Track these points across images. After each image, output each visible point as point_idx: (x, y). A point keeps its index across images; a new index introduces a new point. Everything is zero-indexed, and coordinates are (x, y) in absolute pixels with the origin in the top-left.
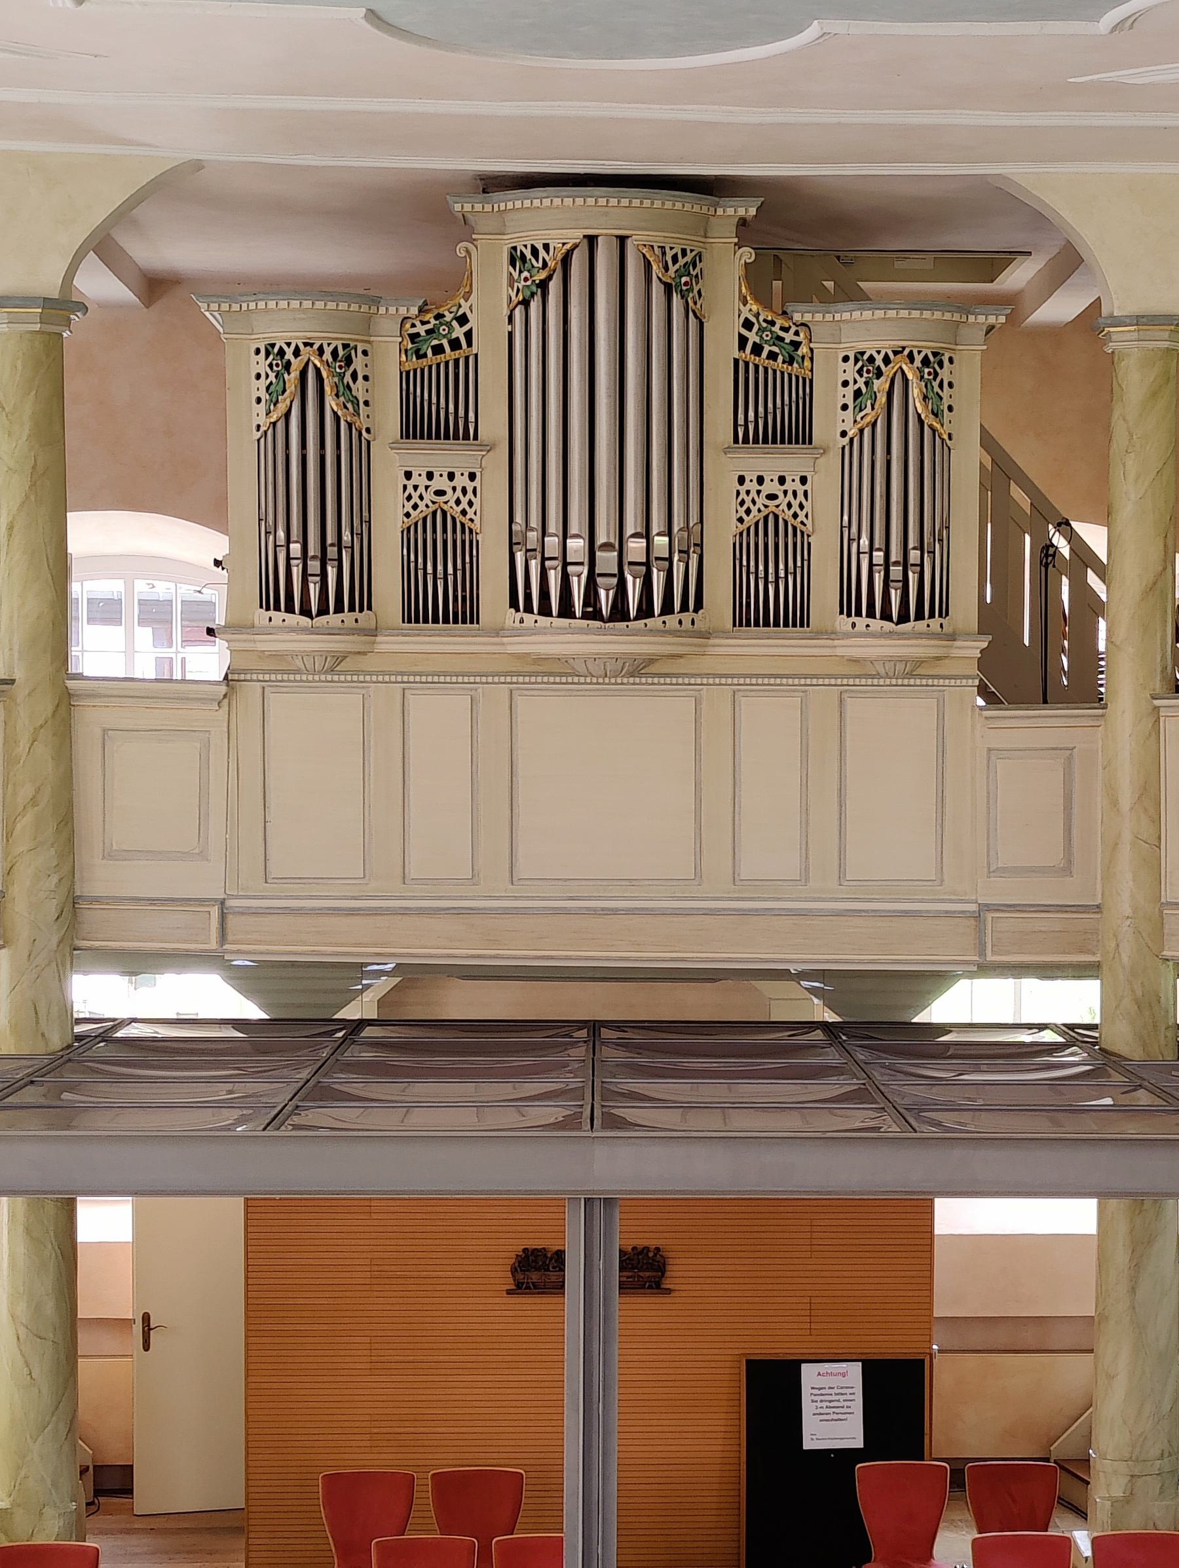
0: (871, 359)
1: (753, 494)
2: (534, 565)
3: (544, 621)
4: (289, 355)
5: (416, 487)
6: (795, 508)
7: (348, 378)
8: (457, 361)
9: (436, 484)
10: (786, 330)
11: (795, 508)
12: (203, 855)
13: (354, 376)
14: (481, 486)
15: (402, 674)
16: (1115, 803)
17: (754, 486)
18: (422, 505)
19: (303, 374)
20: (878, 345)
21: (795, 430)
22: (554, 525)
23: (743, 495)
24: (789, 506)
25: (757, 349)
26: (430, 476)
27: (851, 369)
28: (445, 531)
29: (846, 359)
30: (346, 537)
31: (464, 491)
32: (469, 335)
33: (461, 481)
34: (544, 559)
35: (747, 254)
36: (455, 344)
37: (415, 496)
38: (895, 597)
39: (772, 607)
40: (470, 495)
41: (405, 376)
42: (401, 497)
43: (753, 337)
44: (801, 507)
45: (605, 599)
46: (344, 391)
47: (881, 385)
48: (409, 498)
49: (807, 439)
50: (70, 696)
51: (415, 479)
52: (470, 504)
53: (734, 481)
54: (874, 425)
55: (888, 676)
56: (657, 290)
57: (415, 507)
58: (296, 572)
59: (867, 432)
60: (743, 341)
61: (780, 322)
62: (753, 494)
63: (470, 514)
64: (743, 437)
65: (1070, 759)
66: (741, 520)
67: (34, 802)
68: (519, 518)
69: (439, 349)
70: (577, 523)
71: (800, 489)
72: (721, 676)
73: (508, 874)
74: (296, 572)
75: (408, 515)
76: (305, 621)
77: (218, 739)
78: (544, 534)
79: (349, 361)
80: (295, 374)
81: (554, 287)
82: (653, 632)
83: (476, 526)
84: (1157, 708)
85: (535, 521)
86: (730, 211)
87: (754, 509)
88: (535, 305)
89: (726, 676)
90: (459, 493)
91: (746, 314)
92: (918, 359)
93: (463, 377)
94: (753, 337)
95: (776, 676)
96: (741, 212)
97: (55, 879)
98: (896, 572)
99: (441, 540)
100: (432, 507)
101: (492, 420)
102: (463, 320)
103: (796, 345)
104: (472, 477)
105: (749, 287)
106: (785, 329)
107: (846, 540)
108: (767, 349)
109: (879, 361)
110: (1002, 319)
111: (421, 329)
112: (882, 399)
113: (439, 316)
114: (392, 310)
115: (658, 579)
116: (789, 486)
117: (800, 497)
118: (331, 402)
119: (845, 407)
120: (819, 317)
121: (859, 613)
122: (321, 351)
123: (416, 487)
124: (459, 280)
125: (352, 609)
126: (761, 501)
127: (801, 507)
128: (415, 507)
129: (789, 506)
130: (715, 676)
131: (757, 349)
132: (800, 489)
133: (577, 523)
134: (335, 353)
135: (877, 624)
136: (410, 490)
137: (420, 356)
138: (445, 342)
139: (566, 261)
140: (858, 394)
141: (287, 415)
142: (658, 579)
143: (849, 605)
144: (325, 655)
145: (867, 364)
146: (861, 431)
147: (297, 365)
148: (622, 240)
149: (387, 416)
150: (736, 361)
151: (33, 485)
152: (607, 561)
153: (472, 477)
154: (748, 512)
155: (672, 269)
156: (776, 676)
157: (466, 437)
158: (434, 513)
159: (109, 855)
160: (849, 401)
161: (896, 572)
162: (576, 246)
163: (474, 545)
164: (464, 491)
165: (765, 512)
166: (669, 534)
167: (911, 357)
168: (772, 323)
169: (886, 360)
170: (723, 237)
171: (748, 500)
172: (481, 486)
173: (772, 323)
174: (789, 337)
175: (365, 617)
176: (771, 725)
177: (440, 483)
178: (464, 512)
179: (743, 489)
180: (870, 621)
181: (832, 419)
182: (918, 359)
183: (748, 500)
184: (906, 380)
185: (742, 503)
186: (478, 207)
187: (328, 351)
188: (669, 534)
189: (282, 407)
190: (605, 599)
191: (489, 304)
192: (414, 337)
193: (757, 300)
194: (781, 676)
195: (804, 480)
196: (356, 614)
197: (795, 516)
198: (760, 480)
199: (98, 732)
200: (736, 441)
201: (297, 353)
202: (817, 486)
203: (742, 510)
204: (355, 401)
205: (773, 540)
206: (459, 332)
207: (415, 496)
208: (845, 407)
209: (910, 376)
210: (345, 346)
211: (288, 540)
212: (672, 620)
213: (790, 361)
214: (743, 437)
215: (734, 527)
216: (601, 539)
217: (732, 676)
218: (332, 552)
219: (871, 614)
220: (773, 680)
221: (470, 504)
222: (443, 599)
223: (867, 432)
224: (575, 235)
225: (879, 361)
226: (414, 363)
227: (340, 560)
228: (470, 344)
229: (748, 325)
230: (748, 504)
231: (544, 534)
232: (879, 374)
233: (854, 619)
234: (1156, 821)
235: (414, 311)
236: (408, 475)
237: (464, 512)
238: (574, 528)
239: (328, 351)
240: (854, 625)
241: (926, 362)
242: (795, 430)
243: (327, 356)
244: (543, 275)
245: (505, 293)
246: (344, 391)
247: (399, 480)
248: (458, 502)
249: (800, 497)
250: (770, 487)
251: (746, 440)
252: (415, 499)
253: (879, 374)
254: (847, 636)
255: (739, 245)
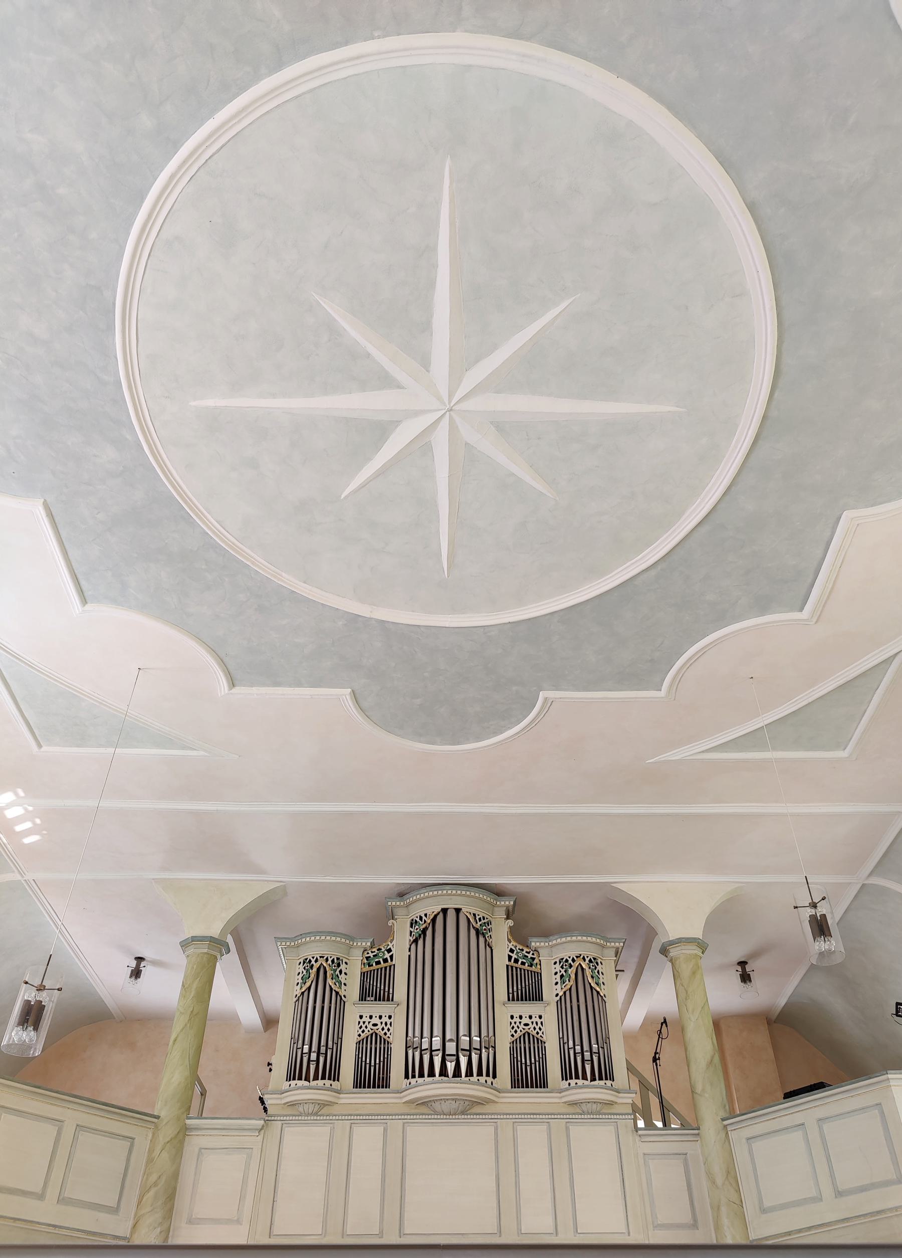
0: (567, 961)
1: (518, 1023)
2: (417, 1054)
3: (421, 1080)
4: (313, 962)
5: (364, 1023)
6: (537, 1029)
7: (338, 972)
8: (386, 968)
9: (374, 1021)
10: (528, 953)
11: (537, 1029)
12: (238, 1222)
13: (341, 972)
14: (394, 1019)
15: (351, 1115)
16: (714, 1182)
17: (518, 1020)
18: (366, 1031)
19: (318, 969)
20: (569, 954)
21: (535, 995)
22: (426, 1033)
23: (513, 1024)
24: (535, 1029)
25: (516, 961)
26: (371, 1017)
27: (558, 966)
28: (376, 1043)
29: (555, 963)
30: (330, 1043)
31: (386, 1024)
32: (391, 957)
33: (384, 1019)
34: (421, 1050)
35: (510, 923)
36: (385, 961)
37: (364, 1026)
38: (588, 1068)
39: (529, 1077)
40: (388, 1026)
41: (363, 974)
42: (357, 1027)
43: (514, 956)
44: (540, 1029)
45: (451, 1066)
46: (335, 977)
47: (572, 971)
48: (361, 1027)
49: (540, 999)
50: (187, 1129)
51: (364, 1019)
52: (389, 1030)
53: (508, 1017)
54: (570, 989)
55: (588, 1114)
56: (473, 932)
57: (363, 1031)
58: (305, 1060)
59: (568, 993)
60: (510, 958)
61: (526, 950)
62: (518, 1023)
63: (388, 1035)
64: (512, 998)
65: (686, 1160)
66: (513, 1036)
67: (155, 1184)
68: (410, 1034)
69: (378, 963)
70: (437, 1030)
71: (539, 1021)
72: (507, 1114)
73: (398, 1231)
74: (305, 1060)
75: (359, 1035)
76: (306, 1083)
77: (256, 1153)
78: (422, 1038)
79: (339, 965)
80: (315, 969)
81: (429, 933)
82: (473, 1083)
83: (390, 1040)
84: (725, 1126)
85: (418, 1033)
86: (503, 903)
87: (518, 1031)
88: (420, 942)
89: (509, 1114)
90: (383, 1025)
91: (511, 946)
92: (587, 960)
93: (388, 972)
94: (514, 956)
95: (534, 1114)
96: (507, 903)
97: (159, 1230)
98: (587, 1055)
99: (374, 1044)
100: (371, 1032)
101: (400, 991)
102: (389, 951)
103: (533, 959)
104: (390, 1017)
105: (512, 935)
106: (528, 953)
107: (562, 1043)
108: (520, 961)
109: (570, 961)
110: (622, 944)
111: (371, 955)
112: (573, 976)
113: (379, 949)
114: (359, 944)
115: (475, 1058)
116: (534, 1019)
117: (539, 1024)
118: (329, 981)
119: (557, 983)
120: (542, 944)
121: (571, 1078)
122: (327, 960)
123: (364, 1023)
124: (389, 933)
125: (329, 1079)
126: (522, 1026)
127: (540, 1029)
128: (363, 1031)
129: (535, 1029)
130: (504, 1114)
131: (516, 961)
132: (539, 1021)
133: (437, 1030)
134: (333, 961)
135: (580, 1082)
136: (361, 1023)
137: (370, 965)
138: (381, 960)
139: (434, 920)
140: (562, 976)
141: (309, 988)
142: (475, 1058)
143: (566, 1075)
144: (314, 1102)
145: (564, 963)
146: (565, 993)
147: (316, 966)
148: (458, 911)
149: (352, 989)
150: (507, 966)
151: (190, 1020)
152: (451, 1048)
153: (390, 1017)
154: (516, 1032)
155: (479, 923)
156: (534, 1114)
157: (388, 1000)
158: (372, 1035)
159: (190, 1221)
160: (558, 980)
161: (587, 1055)
162: (438, 913)
163: (389, 1050)
164: (386, 1024)
165: (524, 1032)
166: (480, 1037)
167: (584, 959)
168: (522, 950)
169: (573, 960)
170: (501, 914)
171: (515, 1026)
172: (394, 1019)
173: (522, 950)
174: (530, 956)
175: (335, 1084)
176: (532, 1140)
177: (375, 1020)
178: (385, 1034)
179: (513, 1021)
180: (577, 1081)
181: (551, 989)
182: (587, 960)
183: (515, 1026)
184: (583, 969)
185: (513, 1028)
186: (398, 903)
187: (330, 960)
188: (480, 1037)
189: (308, 984)
190: (451, 1066)
191: (400, 945)
192: (367, 958)
193: (516, 941)
194: (536, 1114)
195: (540, 1017)
196: (331, 1082)
197: (538, 1033)
198: (521, 1017)
199: (197, 1150)
200: (509, 1000)
201: (316, 961)
202: (545, 1018)
203: (513, 1031)
204: (340, 983)
205: (528, 1044)
206: (387, 956)
207: (364, 1026)
208: (557, 983)
209: (584, 966)
210: (338, 959)
211: (303, 1045)
212: (482, 1079)
213: (531, 965)
214: (512, 998)
215: (510, 1039)
216: (448, 1037)
217: (512, 1114)
218: (323, 1050)
219: (577, 1077)
220: (532, 1116)
221: (389, 1030)
222: (372, 1078)
223: (568, 993)
224: (438, 909)
225: (570, 961)
226: (367, 968)
227: (326, 1054)
228: (392, 960)
229: (512, 951)
230: (516, 1028)
231: (422, 1038)
232: (571, 966)
233: (569, 1081)
234: (738, 1191)
235: (369, 944)
236: (361, 1017)
237: (385, 1034)
238: (435, 1033)
239: (330, 960)
240: (569, 1084)
241: (590, 961)
242: (535, 995)
243: (330, 962)
244: (424, 926)
245: (408, 939)
246: (335, 977)
247: (357, 1018)
248: (383, 1029)
249: (539, 1024)
250: (526, 1020)
251: (513, 1000)
252: (364, 1028)
253: (571, 966)
254: (566, 1090)
255: (508, 918)
